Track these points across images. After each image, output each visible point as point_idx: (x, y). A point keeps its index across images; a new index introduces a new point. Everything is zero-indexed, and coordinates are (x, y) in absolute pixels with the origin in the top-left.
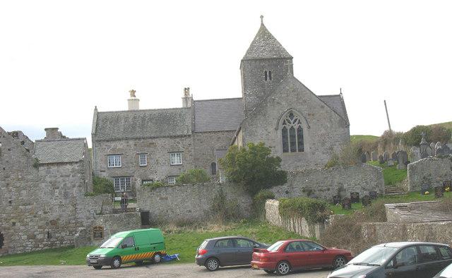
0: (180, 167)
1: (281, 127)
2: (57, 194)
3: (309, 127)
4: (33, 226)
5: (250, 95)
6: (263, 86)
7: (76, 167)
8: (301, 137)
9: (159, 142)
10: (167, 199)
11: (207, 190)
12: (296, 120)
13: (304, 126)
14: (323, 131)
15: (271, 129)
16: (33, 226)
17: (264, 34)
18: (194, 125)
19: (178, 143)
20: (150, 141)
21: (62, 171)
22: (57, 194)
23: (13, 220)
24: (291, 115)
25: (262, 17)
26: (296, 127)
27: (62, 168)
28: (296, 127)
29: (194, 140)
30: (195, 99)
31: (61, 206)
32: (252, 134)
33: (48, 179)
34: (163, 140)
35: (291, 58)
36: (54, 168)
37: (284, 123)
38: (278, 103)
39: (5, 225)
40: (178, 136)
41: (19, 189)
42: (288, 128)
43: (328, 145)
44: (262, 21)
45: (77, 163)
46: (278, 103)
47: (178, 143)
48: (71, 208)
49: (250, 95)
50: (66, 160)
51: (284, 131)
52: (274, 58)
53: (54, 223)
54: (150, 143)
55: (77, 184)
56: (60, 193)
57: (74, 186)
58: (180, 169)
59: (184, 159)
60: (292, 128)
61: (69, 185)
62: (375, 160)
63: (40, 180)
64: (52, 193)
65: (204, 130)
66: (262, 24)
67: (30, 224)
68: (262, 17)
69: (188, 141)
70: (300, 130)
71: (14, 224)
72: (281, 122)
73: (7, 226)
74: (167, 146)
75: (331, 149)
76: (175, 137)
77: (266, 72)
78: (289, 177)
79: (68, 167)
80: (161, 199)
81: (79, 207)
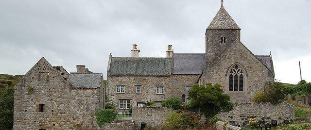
0: (162, 96)
1: (229, 74)
8: (242, 81)
9: (150, 79)
10: (151, 115)
13: (244, 74)
14: (257, 79)
15: (223, 75)
17: (223, 12)
19: (162, 80)
20: (144, 78)
23: (54, 123)
24: (236, 67)
26: (239, 75)
27: (85, 92)
28: (239, 75)
29: (172, 79)
33: (77, 98)
36: (81, 91)
40: (162, 76)
44: (222, 4)
51: (231, 77)
56: (84, 108)
61: (90, 102)
63: (69, 99)
64: (79, 107)
65: (179, 73)
66: (222, 6)
69: (168, 80)
70: (241, 77)
71: (54, 124)
72: (229, 70)
77: (222, 38)
79: (90, 91)
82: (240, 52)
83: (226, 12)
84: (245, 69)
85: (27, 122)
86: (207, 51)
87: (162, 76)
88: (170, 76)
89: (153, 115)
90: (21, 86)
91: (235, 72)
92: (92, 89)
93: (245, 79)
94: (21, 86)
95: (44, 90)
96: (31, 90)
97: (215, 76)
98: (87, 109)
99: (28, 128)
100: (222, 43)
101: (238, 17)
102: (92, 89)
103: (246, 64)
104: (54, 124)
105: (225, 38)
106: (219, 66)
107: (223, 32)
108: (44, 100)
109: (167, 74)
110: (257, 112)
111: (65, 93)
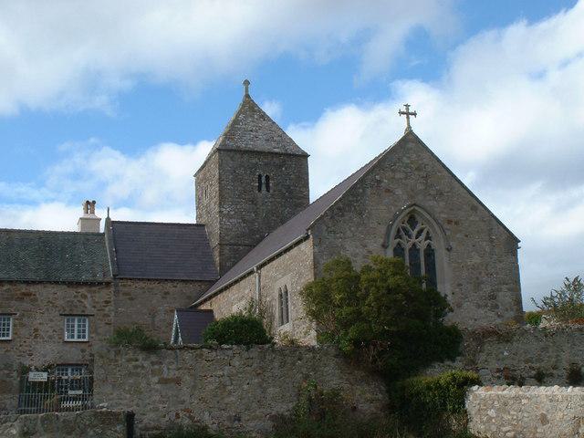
0: (83, 346)
1: (393, 242)
5: (229, 216)
6: (253, 201)
9: (43, 293)
10: (178, 381)
11: (283, 364)
12: (421, 231)
13: (439, 246)
14: (476, 260)
17: (250, 107)
18: (117, 264)
19: (85, 297)
20: (24, 289)
24: (412, 220)
26: (422, 245)
28: (422, 245)
30: (112, 220)
34: (51, 289)
35: (306, 156)
37: (398, 236)
38: (388, 191)
40: (85, 284)
42: (407, 246)
43: (487, 289)
44: (247, 90)
46: (388, 191)
47: (85, 297)
49: (229, 216)
52: (276, 153)
54: (24, 294)
58: (83, 351)
59: (94, 330)
60: (414, 248)
66: (247, 96)
68: (247, 83)
69: (103, 294)
70: (430, 253)
72: (393, 232)
74: (60, 302)
75: (493, 297)
76: (79, 284)
77: (260, 176)
78: (467, 343)
80: (164, 381)
82: (422, 173)
83: (260, 111)
84: (441, 227)
87: (85, 284)
88: (108, 284)
91: (410, 237)
93: (442, 258)
100: (260, 190)
105: (267, 177)
106: (361, 214)
109: (99, 277)
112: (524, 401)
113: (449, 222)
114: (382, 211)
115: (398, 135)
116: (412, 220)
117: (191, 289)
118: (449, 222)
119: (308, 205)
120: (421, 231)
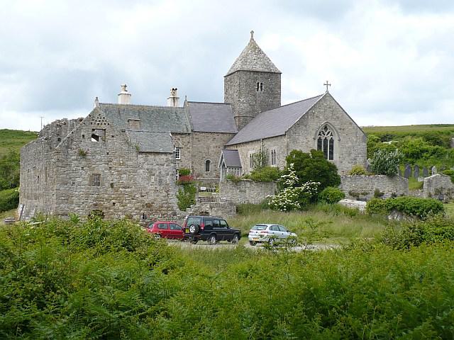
2: (153, 180)
3: (339, 140)
4: (131, 207)
7: (170, 157)
8: (332, 147)
10: (245, 191)
12: (329, 133)
15: (311, 138)
16: (131, 207)
17: (254, 47)
21: (158, 160)
22: (153, 180)
23: (114, 201)
24: (326, 128)
25: (252, 32)
26: (329, 139)
27: (158, 157)
28: (329, 139)
29: (193, 138)
31: (156, 191)
32: (295, 141)
33: (146, 167)
36: (151, 157)
39: (106, 204)
41: (120, 173)
42: (323, 138)
43: (353, 156)
44: (252, 36)
45: (170, 154)
48: (165, 194)
50: (161, 150)
51: (319, 141)
53: (149, 206)
55: (170, 173)
56: (155, 180)
57: (168, 174)
61: (163, 173)
62: (400, 171)
63: (138, 166)
64: (149, 179)
65: (202, 130)
66: (252, 39)
67: (128, 205)
68: (252, 32)
69: (187, 139)
70: (332, 141)
71: (114, 204)
73: (108, 205)
79: (163, 156)
81: (171, 193)
84: (337, 131)
85: (75, 200)
86: (226, 98)
88: (189, 134)
89: (247, 191)
90: (67, 147)
92: (165, 153)
94: (67, 147)
95: (100, 154)
96: (83, 154)
97: (301, 139)
98: (160, 181)
99: (76, 208)
101: (275, 51)
102: (165, 153)
103: (337, 124)
104: (114, 204)
106: (306, 126)
107: (259, 76)
108: (101, 168)
109: (185, 131)
110: (369, 187)
111: (131, 160)
112: (361, 279)
113: (340, 129)
114: (315, 125)
115: (324, 92)
116: (326, 128)
117: (226, 137)
118: (340, 129)
119: (278, 105)
120: (329, 133)
